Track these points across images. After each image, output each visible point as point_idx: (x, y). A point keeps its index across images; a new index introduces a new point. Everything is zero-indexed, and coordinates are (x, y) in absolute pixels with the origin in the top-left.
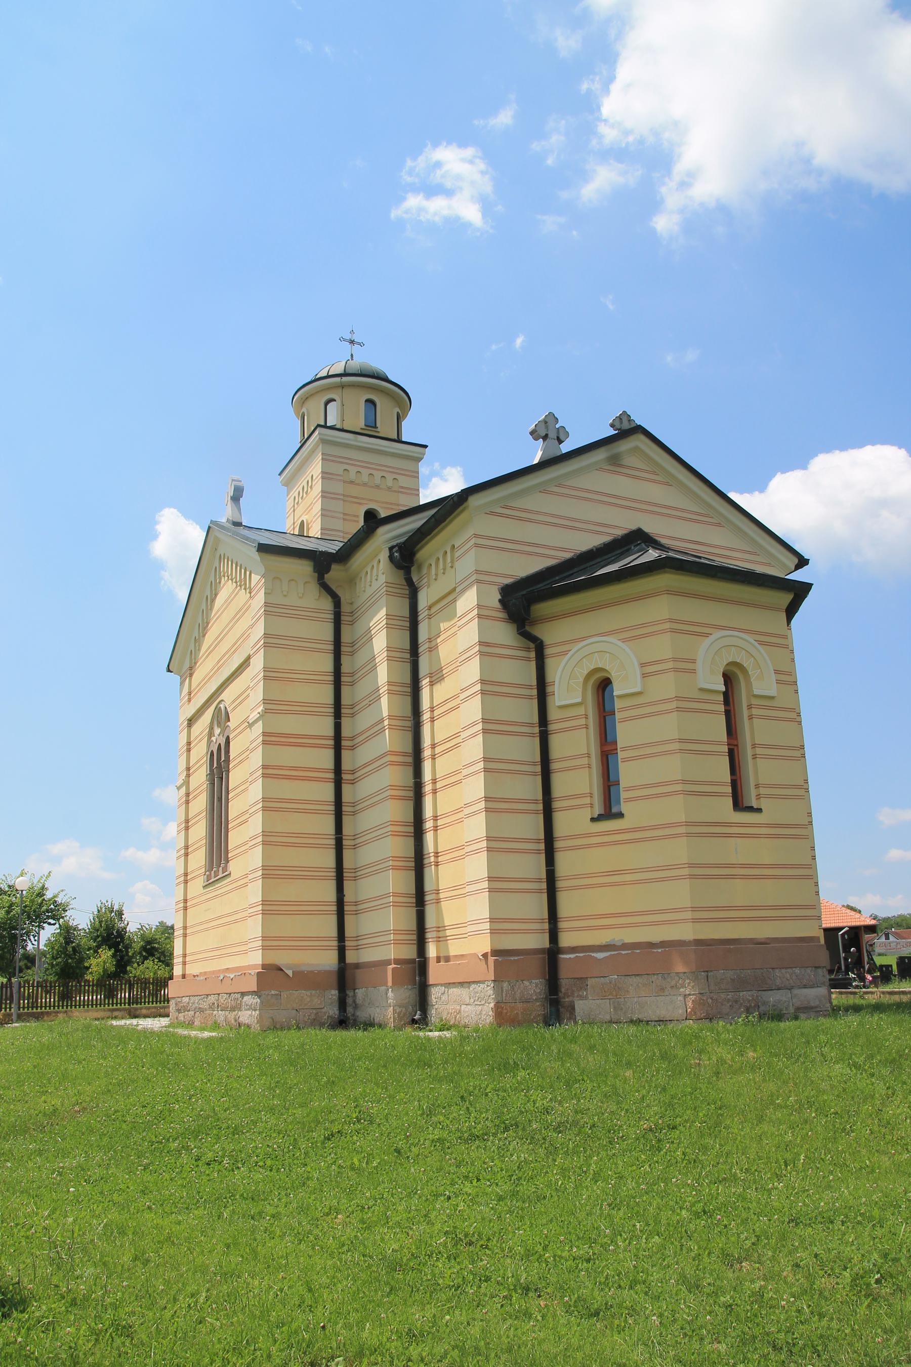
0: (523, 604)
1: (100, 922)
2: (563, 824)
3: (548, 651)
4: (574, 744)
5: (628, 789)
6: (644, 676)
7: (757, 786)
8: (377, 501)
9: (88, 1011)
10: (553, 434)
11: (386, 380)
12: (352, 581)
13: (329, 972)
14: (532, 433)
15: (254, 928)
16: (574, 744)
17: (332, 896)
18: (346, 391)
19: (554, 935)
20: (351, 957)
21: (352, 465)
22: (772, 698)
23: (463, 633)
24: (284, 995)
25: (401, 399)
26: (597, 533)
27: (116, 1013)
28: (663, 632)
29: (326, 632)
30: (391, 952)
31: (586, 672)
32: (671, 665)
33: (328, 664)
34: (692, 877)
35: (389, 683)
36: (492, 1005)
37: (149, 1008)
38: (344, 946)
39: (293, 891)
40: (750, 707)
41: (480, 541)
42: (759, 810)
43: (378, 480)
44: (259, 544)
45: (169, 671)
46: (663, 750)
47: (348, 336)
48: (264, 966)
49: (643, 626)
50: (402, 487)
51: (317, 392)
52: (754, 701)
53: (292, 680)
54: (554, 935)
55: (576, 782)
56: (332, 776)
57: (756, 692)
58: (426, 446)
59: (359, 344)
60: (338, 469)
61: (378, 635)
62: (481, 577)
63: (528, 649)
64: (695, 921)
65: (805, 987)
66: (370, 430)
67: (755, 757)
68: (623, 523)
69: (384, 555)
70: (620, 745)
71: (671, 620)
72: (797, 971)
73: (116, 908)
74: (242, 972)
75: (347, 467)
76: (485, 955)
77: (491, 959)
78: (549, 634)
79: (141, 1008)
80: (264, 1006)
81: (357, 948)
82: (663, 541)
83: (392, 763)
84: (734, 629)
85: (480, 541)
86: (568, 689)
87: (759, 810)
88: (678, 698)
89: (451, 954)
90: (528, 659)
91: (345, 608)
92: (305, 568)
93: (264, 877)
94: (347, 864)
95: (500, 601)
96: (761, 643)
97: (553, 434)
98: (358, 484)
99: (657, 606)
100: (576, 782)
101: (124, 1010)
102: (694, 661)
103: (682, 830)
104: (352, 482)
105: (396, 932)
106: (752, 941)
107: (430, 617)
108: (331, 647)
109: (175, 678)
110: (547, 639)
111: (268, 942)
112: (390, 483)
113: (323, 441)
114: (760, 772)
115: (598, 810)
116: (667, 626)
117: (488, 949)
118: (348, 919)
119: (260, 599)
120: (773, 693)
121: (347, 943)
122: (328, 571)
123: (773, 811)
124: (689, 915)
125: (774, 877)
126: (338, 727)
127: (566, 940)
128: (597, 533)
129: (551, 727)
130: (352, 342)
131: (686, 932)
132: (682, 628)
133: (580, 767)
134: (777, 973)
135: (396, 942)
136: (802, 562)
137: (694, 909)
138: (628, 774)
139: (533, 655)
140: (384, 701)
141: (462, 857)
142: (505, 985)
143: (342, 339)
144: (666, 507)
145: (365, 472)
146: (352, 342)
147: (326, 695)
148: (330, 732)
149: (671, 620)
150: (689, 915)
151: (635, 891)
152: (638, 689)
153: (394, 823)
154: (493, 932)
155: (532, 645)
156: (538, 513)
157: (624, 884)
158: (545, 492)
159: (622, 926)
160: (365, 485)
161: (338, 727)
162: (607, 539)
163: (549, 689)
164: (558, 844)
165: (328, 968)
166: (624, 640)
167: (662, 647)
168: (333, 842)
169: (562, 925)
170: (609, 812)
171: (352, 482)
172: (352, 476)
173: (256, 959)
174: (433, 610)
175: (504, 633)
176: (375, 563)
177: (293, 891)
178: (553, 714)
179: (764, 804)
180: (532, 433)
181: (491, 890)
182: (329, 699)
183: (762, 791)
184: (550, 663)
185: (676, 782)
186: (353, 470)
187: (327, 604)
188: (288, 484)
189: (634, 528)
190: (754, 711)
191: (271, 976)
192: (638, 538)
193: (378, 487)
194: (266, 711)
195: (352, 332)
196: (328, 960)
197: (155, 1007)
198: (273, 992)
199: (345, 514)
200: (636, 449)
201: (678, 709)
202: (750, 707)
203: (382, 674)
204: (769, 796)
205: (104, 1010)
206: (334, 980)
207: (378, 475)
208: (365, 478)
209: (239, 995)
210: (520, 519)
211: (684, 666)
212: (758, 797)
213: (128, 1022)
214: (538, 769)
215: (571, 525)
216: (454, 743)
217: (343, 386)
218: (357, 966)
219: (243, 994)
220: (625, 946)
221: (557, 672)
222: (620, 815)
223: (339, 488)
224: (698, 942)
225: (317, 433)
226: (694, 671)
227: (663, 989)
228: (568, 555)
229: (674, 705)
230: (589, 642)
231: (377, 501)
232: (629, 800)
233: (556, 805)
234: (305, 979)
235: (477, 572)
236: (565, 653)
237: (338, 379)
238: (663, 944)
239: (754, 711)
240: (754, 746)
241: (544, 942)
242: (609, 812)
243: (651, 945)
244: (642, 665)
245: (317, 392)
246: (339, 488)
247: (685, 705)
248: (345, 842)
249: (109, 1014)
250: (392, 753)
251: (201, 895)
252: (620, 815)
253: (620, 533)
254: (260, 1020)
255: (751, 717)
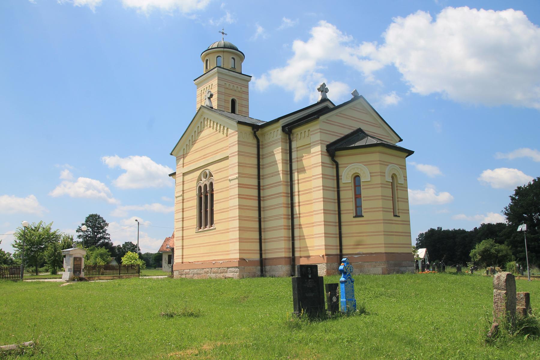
0: (333, 150)
1: (65, 243)
2: (344, 218)
3: (340, 166)
4: (348, 194)
6: (371, 176)
7: (398, 210)
10: (324, 90)
11: (237, 50)
12: (263, 135)
14: (318, 89)
15: (237, 246)
16: (348, 194)
18: (225, 54)
19: (341, 250)
20: (264, 257)
23: (313, 159)
24: (246, 268)
25: (241, 56)
28: (377, 164)
29: (255, 151)
32: (379, 174)
34: (384, 235)
35: (283, 171)
39: (247, 235)
40: (397, 187)
41: (321, 131)
42: (399, 216)
43: (235, 88)
45: (171, 154)
46: (374, 199)
47: (222, 31)
48: (240, 259)
52: (399, 185)
53: (246, 167)
54: (341, 250)
55: (348, 206)
56: (257, 198)
60: (223, 83)
61: (278, 155)
62: (322, 142)
63: (333, 165)
66: (233, 70)
67: (398, 201)
68: (356, 126)
69: (280, 129)
71: (380, 161)
73: (70, 237)
74: (230, 261)
76: (323, 256)
77: (325, 257)
78: (341, 161)
80: (240, 271)
81: (265, 253)
83: (284, 196)
85: (321, 131)
86: (346, 178)
87: (399, 216)
90: (333, 168)
91: (261, 143)
97: (324, 90)
99: (375, 156)
100: (348, 206)
102: (385, 173)
103: (382, 221)
104: (227, 88)
106: (397, 253)
109: (174, 158)
110: (339, 162)
111: (241, 251)
112: (239, 89)
115: (355, 215)
116: (379, 162)
119: (235, 138)
120: (403, 183)
123: (402, 217)
124: (383, 245)
125: (396, 235)
126: (259, 183)
130: (223, 33)
131: (383, 250)
132: (384, 163)
133: (401, 210)
135: (285, 252)
136: (401, 140)
138: (365, 205)
139: (335, 166)
140: (281, 175)
143: (226, 34)
145: (232, 85)
146: (223, 33)
148: (256, 184)
149: (380, 161)
151: (368, 237)
153: (284, 215)
154: (326, 249)
155: (334, 163)
159: (373, 248)
160: (231, 90)
161: (259, 183)
162: (352, 131)
163: (340, 178)
164: (342, 224)
166: (365, 165)
167: (377, 168)
169: (343, 247)
170: (359, 215)
171: (227, 88)
172: (227, 86)
173: (237, 256)
175: (328, 160)
176: (276, 130)
177: (247, 235)
178: (341, 185)
179: (400, 215)
180: (318, 89)
182: (256, 173)
183: (400, 211)
184: (340, 170)
185: (380, 208)
186: (228, 84)
187: (255, 142)
188: (198, 85)
192: (360, 131)
193: (235, 91)
194: (239, 176)
196: (257, 257)
202: (397, 187)
203: (280, 167)
204: (402, 213)
206: (259, 263)
207: (236, 86)
208: (231, 87)
210: (331, 124)
211: (383, 174)
212: (399, 213)
214: (336, 201)
217: (224, 52)
218: (265, 259)
219: (228, 268)
220: (363, 254)
222: (362, 216)
223: (223, 90)
224: (386, 253)
225: (216, 69)
226: (384, 176)
228: (343, 136)
229: (380, 185)
230: (351, 165)
232: (365, 212)
233: (342, 212)
234: (252, 263)
235: (321, 140)
236: (346, 167)
237: (222, 49)
238: (375, 253)
240: (398, 198)
241: (338, 252)
242: (359, 215)
244: (370, 173)
246: (223, 90)
249: (112, 278)
252: (362, 216)
255: (397, 190)
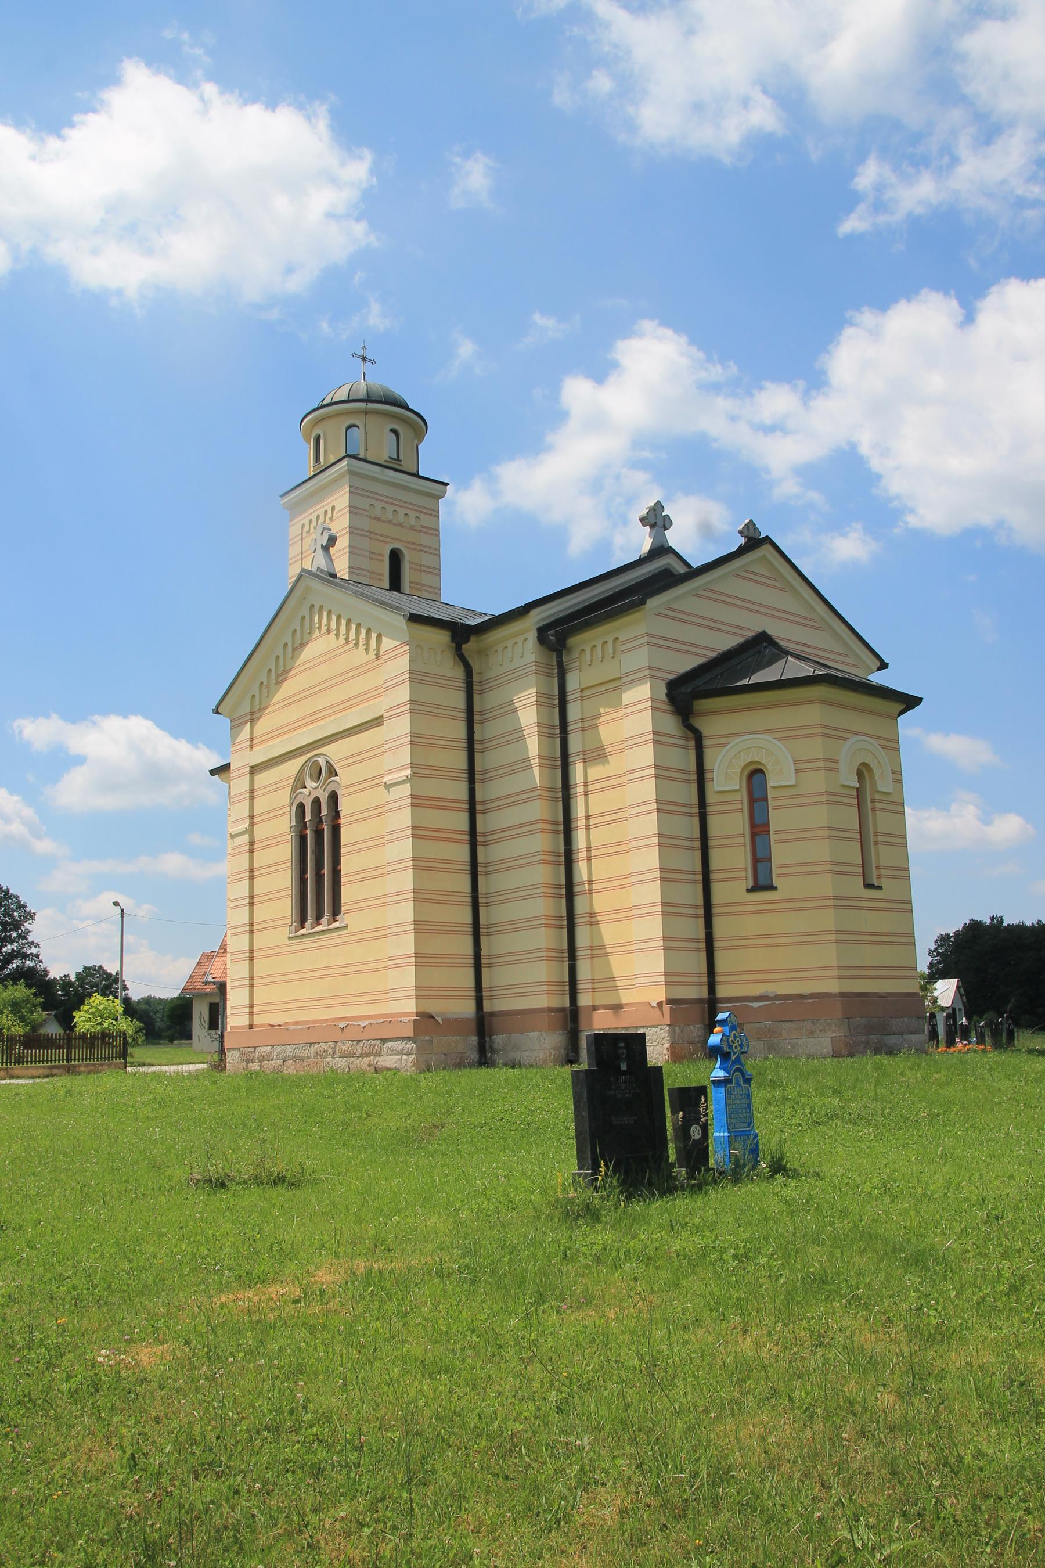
0: (688, 696)
3: (706, 742)
4: (730, 825)
5: (780, 866)
6: (797, 771)
8: (401, 541)
9: (27, 1068)
10: (660, 523)
11: (406, 407)
12: (483, 653)
13: (468, 1019)
14: (642, 520)
15: (408, 977)
16: (730, 825)
17: (469, 950)
19: (712, 987)
20: (487, 1007)
21: (379, 500)
22: (889, 794)
24: (435, 1040)
25: (418, 425)
26: (734, 634)
27: (55, 1071)
29: (459, 700)
30: (543, 1002)
31: (743, 764)
33: (461, 732)
35: (540, 757)
36: (667, 1045)
37: (87, 1065)
38: (482, 996)
40: (873, 801)
42: (880, 888)
43: (401, 518)
44: (411, 614)
45: (216, 711)
46: (807, 836)
47: (361, 352)
48: (418, 1014)
49: (798, 728)
50: (424, 527)
51: (343, 414)
52: (877, 796)
54: (712, 987)
55: (732, 858)
57: (879, 789)
58: (447, 484)
59: (370, 361)
63: (686, 739)
64: (840, 977)
65: (911, 1033)
66: (394, 465)
67: (876, 843)
69: (532, 636)
70: (772, 828)
71: (822, 726)
72: (906, 1020)
74: (389, 1020)
75: (373, 502)
76: (660, 1004)
78: (710, 727)
79: (80, 1066)
80: (420, 1050)
82: (782, 643)
83: (544, 831)
84: (868, 735)
86: (726, 778)
87: (880, 888)
88: (828, 793)
89: (624, 1001)
90: (687, 748)
92: (443, 637)
93: (416, 931)
94: (482, 921)
95: (667, 695)
96: (883, 747)
97: (660, 523)
98: (382, 521)
100: (732, 858)
101: (63, 1067)
102: (837, 761)
104: (377, 519)
105: (548, 983)
107: (582, 699)
108: (464, 715)
109: (223, 722)
111: (421, 992)
112: (413, 522)
113: (352, 473)
114: (883, 856)
115: (750, 884)
117: (662, 997)
118: (485, 971)
121: (484, 994)
122: (467, 641)
123: (890, 888)
124: (835, 972)
127: (722, 992)
128: (734, 634)
129: (709, 809)
130: (364, 359)
131: (833, 987)
132: (835, 734)
134: (894, 1021)
135: (549, 993)
136: (883, 666)
137: (839, 968)
138: (780, 854)
139: (692, 743)
140: (536, 770)
141: (631, 918)
142: (677, 1029)
143: (373, 362)
144: (782, 611)
145: (390, 508)
147: (460, 760)
149: (822, 726)
150: (835, 972)
151: (781, 952)
152: (792, 782)
156: (693, 615)
157: (777, 945)
158: (697, 595)
160: (389, 522)
162: (740, 640)
163: (707, 776)
165: (467, 1016)
166: (779, 739)
167: (815, 748)
168: (469, 900)
170: (762, 884)
171: (377, 519)
172: (377, 511)
174: (585, 693)
175: (671, 724)
176: (520, 640)
178: (711, 798)
179: (883, 882)
180: (642, 520)
181: (666, 948)
183: (882, 872)
184: (709, 754)
187: (459, 673)
189: (760, 630)
190: (878, 805)
191: (424, 1020)
194: (414, 774)
195: (364, 348)
196: (467, 1008)
197: (93, 1065)
198: (427, 1038)
199: (371, 553)
200: (764, 557)
201: (828, 802)
202: (873, 801)
203: (533, 746)
204: (887, 877)
205: (44, 1067)
206: (473, 1026)
207: (402, 512)
208: (389, 516)
209: (378, 1042)
211: (831, 765)
212: (879, 876)
213: (8, 1081)
215: (714, 626)
216: (617, 816)
217: (366, 412)
218: (492, 1014)
219: (384, 1041)
220: (777, 997)
221: (717, 761)
222: (772, 888)
224: (843, 995)
225: (345, 463)
226: (837, 770)
227: (812, 1033)
228: (714, 655)
231: (401, 541)
232: (780, 876)
234: (452, 1025)
235: (650, 668)
236: (725, 745)
237: (363, 405)
238: (812, 996)
239: (878, 805)
240: (876, 834)
241: (705, 994)
242: (762, 884)
243: (801, 997)
244: (796, 762)
245: (343, 414)
247: (832, 798)
248: (480, 900)
249: (47, 1072)
250: (543, 821)
251: (286, 945)
253: (750, 634)
254: (416, 1064)
255: (874, 810)
